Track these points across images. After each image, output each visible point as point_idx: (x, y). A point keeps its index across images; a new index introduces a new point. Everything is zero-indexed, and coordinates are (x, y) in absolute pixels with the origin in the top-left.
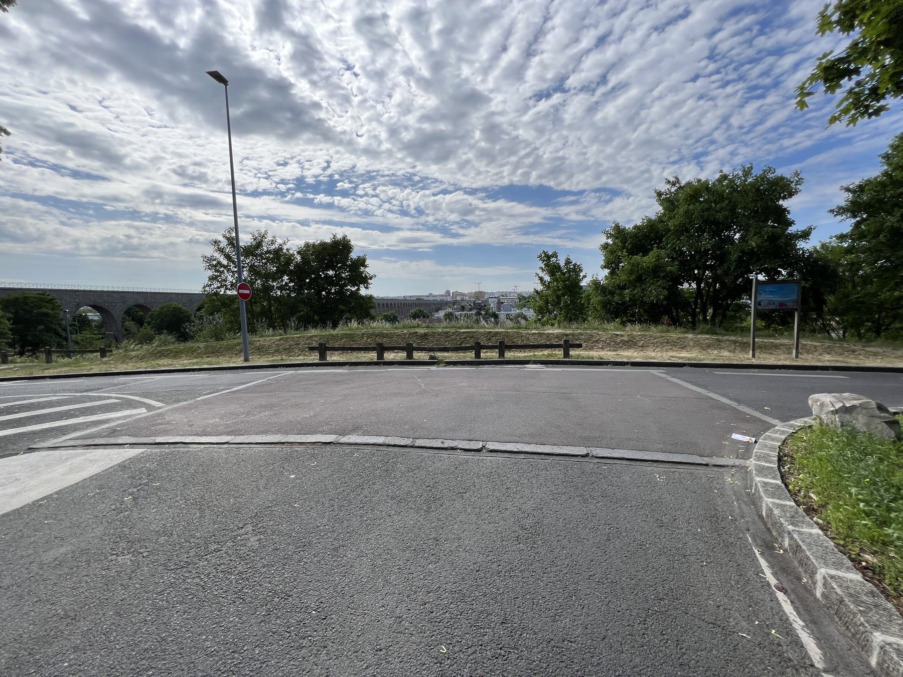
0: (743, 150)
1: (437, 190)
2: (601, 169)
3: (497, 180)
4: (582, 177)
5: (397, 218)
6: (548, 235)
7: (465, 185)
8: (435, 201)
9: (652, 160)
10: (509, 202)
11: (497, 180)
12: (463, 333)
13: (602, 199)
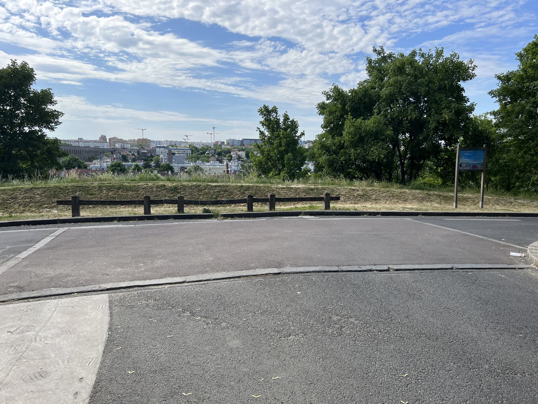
0: (398, 20)
1: (89, 9)
2: (277, 17)
3: (165, 10)
4: (257, 22)
5: (32, 37)
6: (222, 81)
7: (125, 9)
8: (86, 23)
9: (324, 16)
10: (178, 38)
11: (165, 10)
12: (215, 186)
13: (277, 49)
